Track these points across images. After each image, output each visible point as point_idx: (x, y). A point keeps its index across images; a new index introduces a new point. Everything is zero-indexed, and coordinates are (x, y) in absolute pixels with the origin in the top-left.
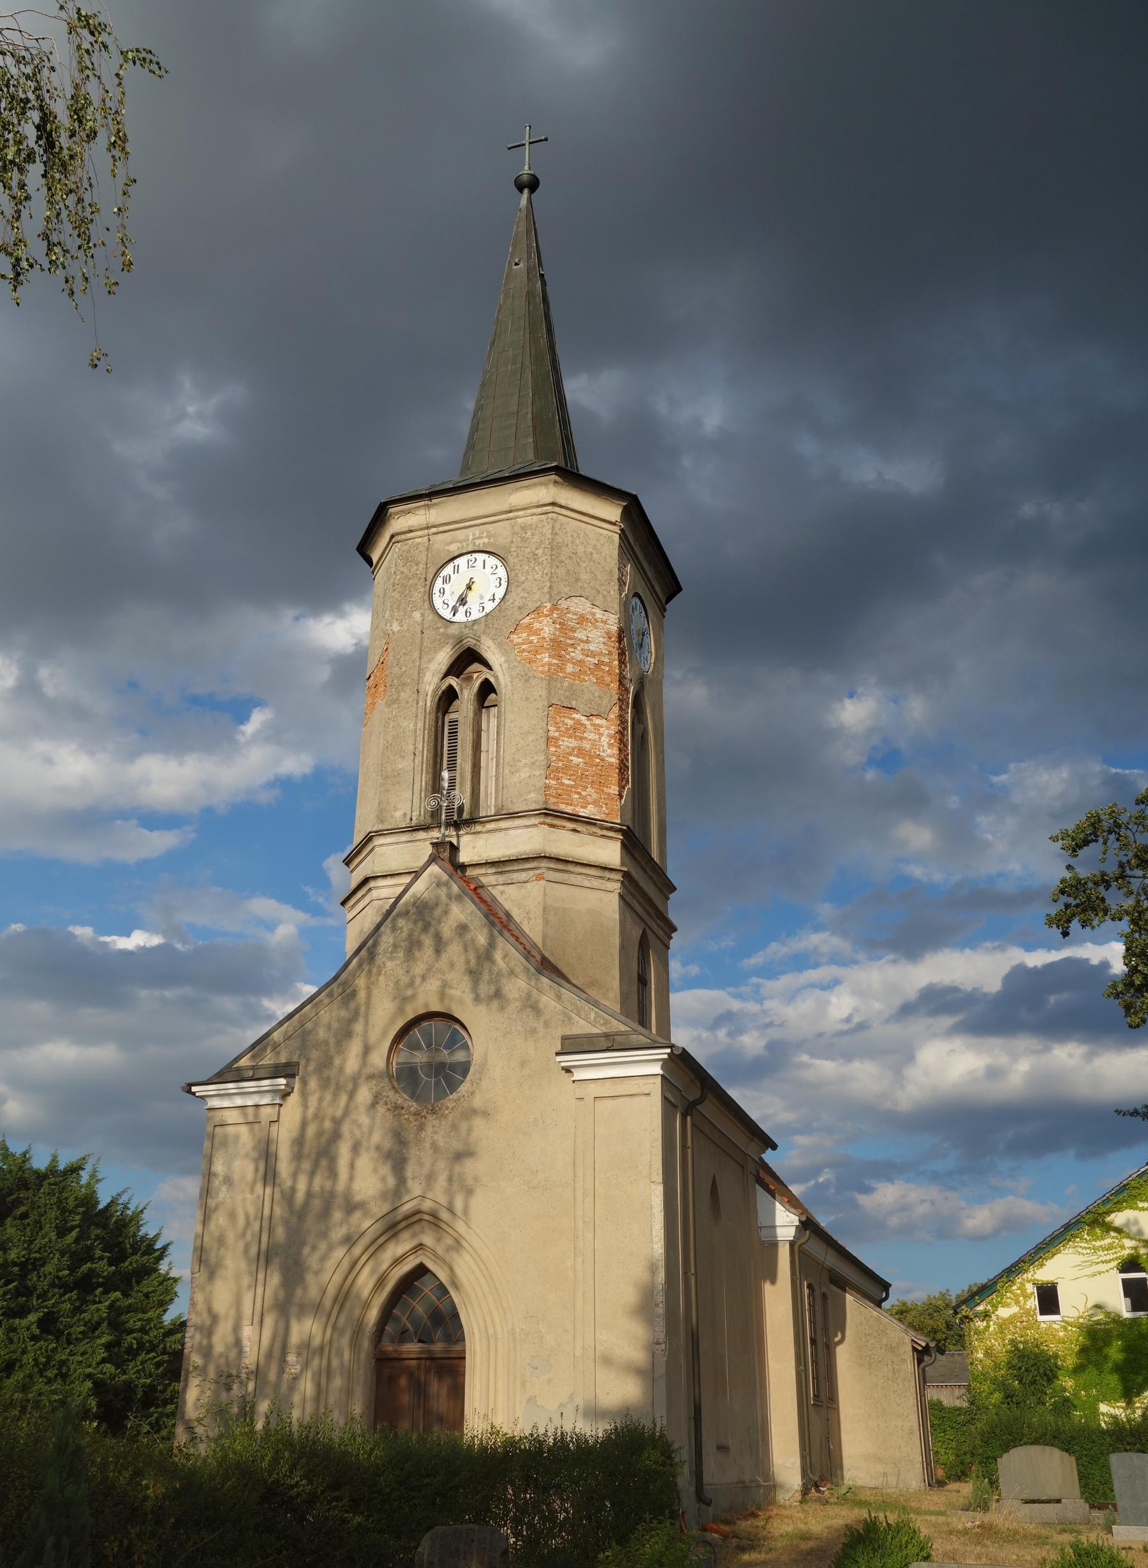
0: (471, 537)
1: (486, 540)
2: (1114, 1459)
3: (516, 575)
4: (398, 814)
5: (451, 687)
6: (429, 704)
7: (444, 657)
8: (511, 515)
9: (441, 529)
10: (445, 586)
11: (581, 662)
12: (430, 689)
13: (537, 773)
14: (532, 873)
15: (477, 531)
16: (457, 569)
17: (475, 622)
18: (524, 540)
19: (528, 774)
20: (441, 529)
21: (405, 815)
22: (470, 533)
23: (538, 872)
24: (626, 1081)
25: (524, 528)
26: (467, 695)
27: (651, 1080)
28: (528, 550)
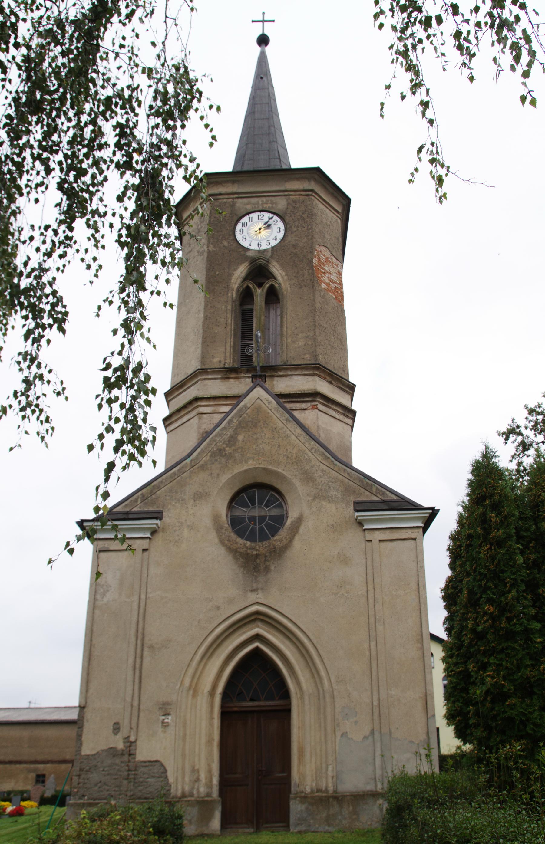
0: (260, 203)
1: (270, 205)
2: (83, 753)
3: (291, 227)
4: (216, 360)
5: (248, 287)
6: (234, 296)
7: (242, 270)
8: (286, 193)
9: (241, 196)
10: (244, 228)
11: (328, 284)
12: (235, 287)
13: (310, 343)
14: (309, 404)
15: (264, 199)
16: (251, 220)
17: (265, 251)
18: (294, 208)
19: (303, 343)
20: (241, 196)
21: (220, 362)
22: (260, 200)
23: (314, 403)
24: (400, 531)
25: (294, 202)
26: (259, 294)
27: (417, 530)
28: (298, 214)
